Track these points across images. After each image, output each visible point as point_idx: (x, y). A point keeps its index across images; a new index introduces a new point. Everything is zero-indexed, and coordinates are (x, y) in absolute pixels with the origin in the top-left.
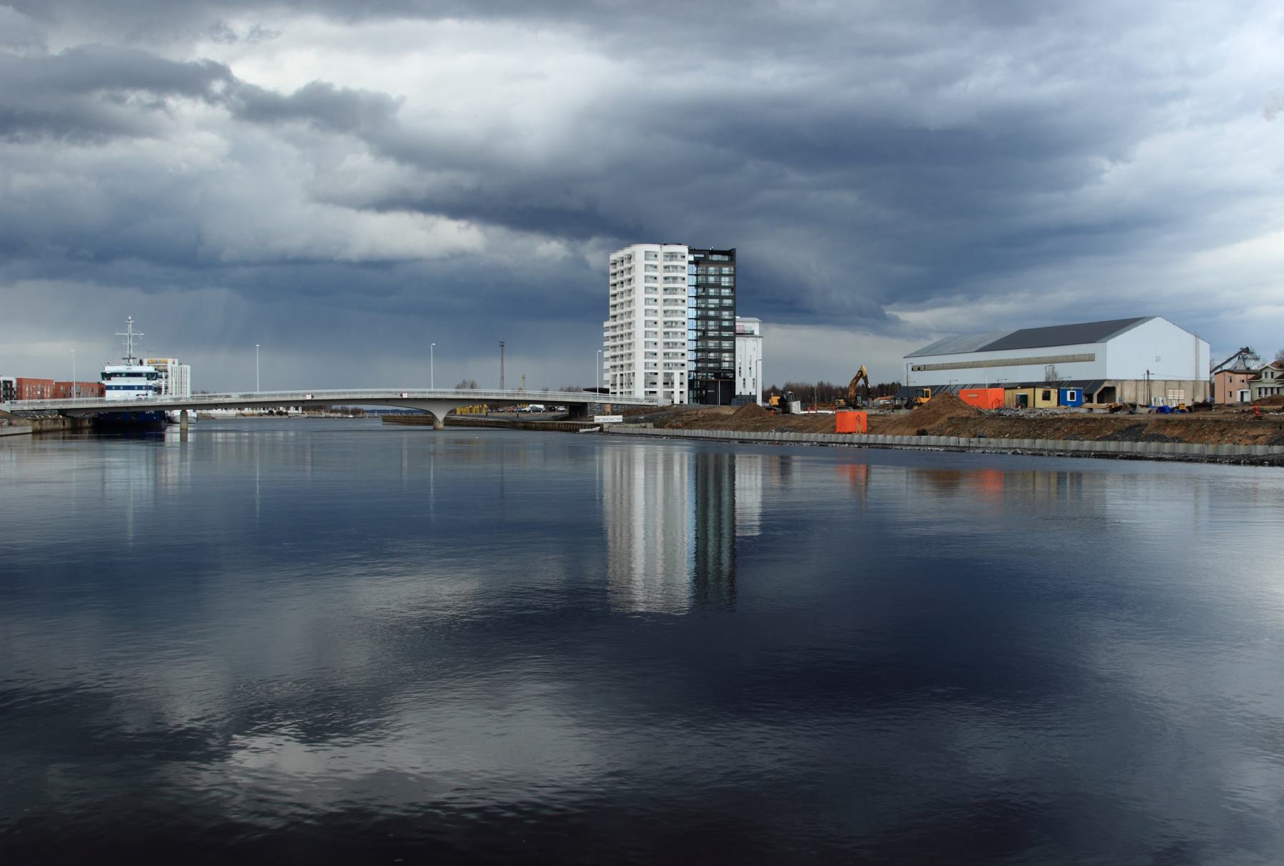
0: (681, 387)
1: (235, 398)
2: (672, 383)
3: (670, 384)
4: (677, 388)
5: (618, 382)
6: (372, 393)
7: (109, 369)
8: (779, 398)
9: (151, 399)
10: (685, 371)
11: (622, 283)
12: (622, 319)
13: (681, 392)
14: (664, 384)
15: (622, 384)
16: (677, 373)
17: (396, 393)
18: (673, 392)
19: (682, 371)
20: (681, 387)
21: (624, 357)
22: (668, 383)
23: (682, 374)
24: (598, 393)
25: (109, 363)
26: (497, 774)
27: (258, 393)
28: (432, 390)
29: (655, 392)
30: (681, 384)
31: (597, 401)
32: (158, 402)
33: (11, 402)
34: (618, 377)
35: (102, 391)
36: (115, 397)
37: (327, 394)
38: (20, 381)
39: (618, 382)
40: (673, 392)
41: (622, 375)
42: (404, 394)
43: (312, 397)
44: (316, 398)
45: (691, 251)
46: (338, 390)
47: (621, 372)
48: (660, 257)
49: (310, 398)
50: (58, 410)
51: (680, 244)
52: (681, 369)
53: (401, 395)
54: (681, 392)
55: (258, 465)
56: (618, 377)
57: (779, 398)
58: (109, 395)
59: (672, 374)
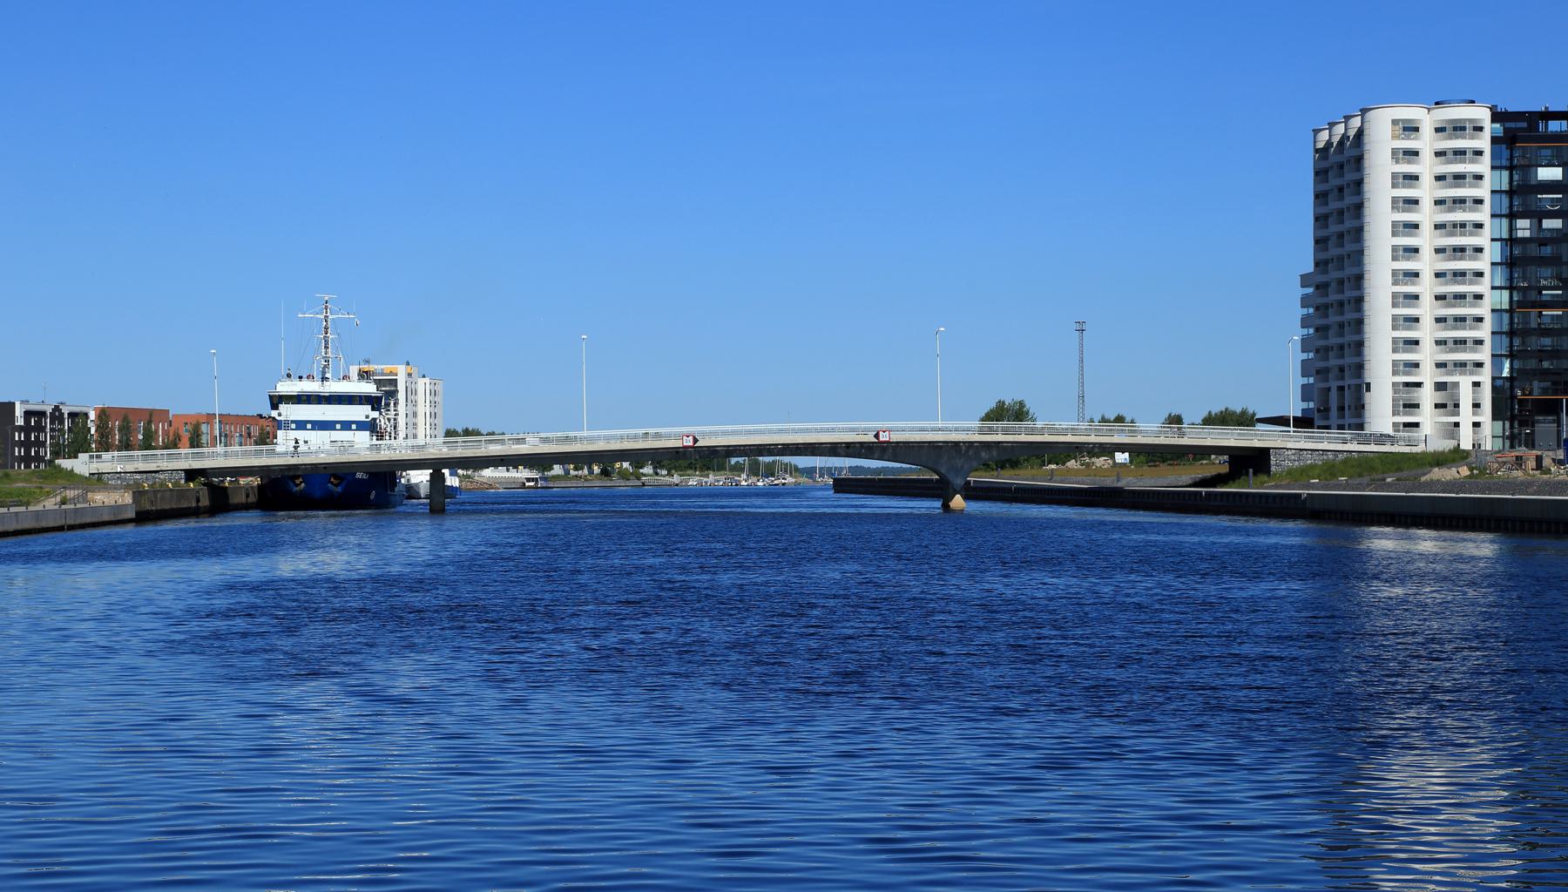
0: (1474, 414)
1: (532, 446)
2: (1457, 406)
3: (1450, 408)
4: (1466, 416)
5: (1334, 404)
6: (817, 431)
7: (286, 387)
8: (431, 471)
9: (361, 447)
10: (1485, 377)
11: (1341, 190)
12: (1342, 335)
13: (1476, 425)
14: (1437, 406)
15: (1341, 408)
16: (1465, 382)
17: (865, 431)
18: (1457, 425)
19: (1476, 379)
20: (1474, 414)
21: (1346, 351)
22: (1451, 403)
23: (1476, 384)
24: (1292, 429)
25: (289, 376)
26: (1198, 860)
27: (585, 433)
28: (940, 424)
29: (1416, 425)
30: (1476, 406)
31: (1290, 445)
32: (385, 455)
33: (91, 457)
34: (1334, 394)
35: (266, 438)
36: (288, 448)
37: (795, 431)
38: (103, 414)
39: (1334, 404)
40: (1457, 425)
41: (1341, 389)
42: (881, 433)
43: (696, 440)
44: (884, 437)
45: (1497, 116)
46: (770, 426)
47: (1340, 383)
48: (1427, 130)
49: (691, 444)
50: (185, 471)
51: (1473, 102)
52: (1472, 373)
53: (877, 436)
54: (1476, 425)
55: (1517, 407)
56: (1334, 394)
57: (431, 471)
58: (284, 440)
59: (1456, 385)
